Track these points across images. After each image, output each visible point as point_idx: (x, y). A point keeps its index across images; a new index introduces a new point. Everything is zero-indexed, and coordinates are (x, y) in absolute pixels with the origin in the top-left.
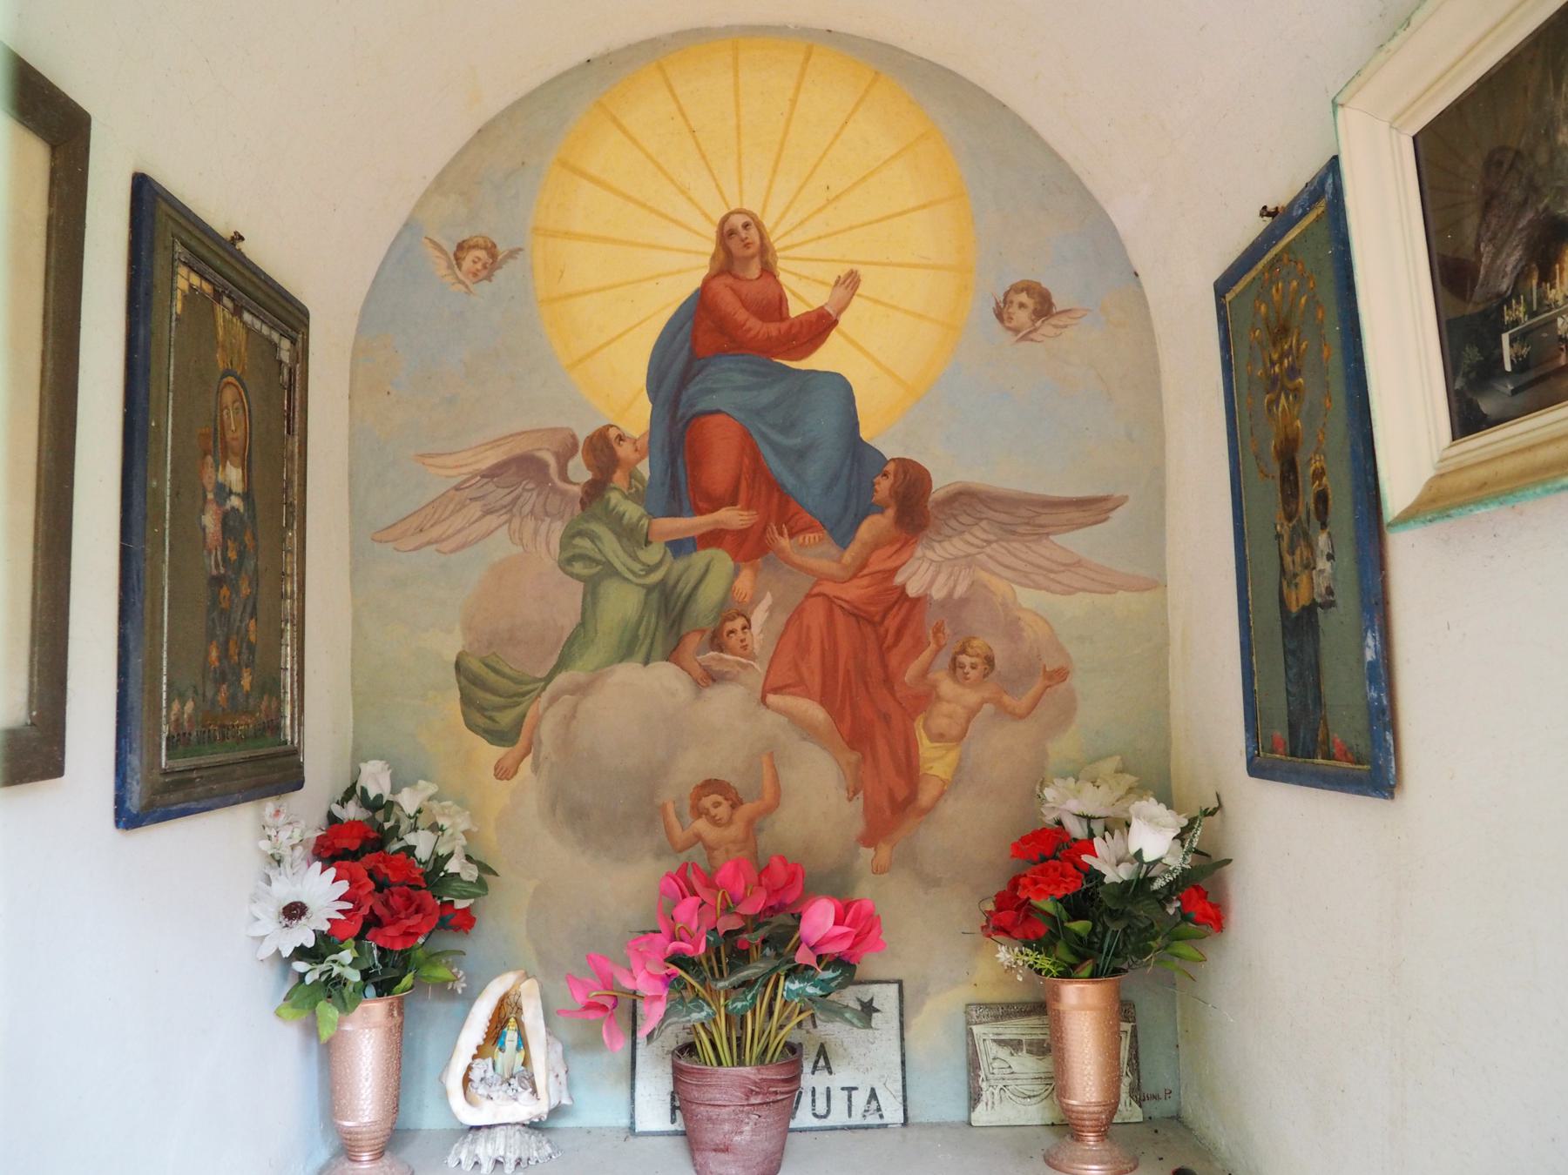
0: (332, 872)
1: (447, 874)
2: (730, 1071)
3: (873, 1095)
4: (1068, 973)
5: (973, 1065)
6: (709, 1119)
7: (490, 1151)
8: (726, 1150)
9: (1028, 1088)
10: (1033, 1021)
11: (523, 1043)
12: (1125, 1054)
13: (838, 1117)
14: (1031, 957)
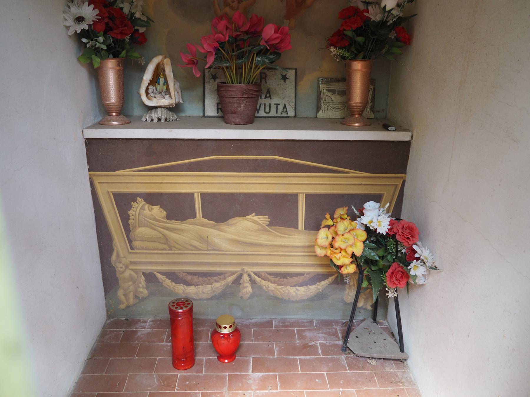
0: (92, 6)
1: (136, 18)
2: (236, 86)
3: (285, 107)
4: (355, 58)
5: (319, 98)
6: (230, 102)
7: (156, 116)
8: (235, 113)
9: (336, 106)
10: (341, 84)
11: (166, 82)
12: (370, 96)
13: (273, 113)
14: (341, 52)
